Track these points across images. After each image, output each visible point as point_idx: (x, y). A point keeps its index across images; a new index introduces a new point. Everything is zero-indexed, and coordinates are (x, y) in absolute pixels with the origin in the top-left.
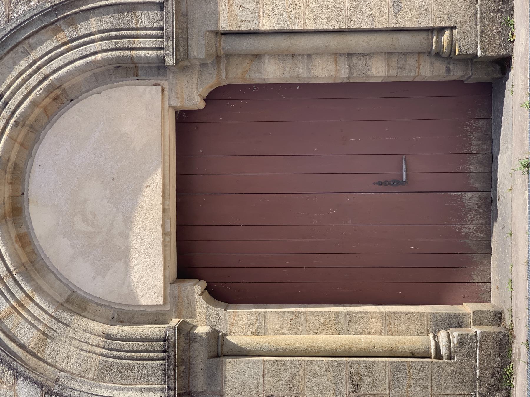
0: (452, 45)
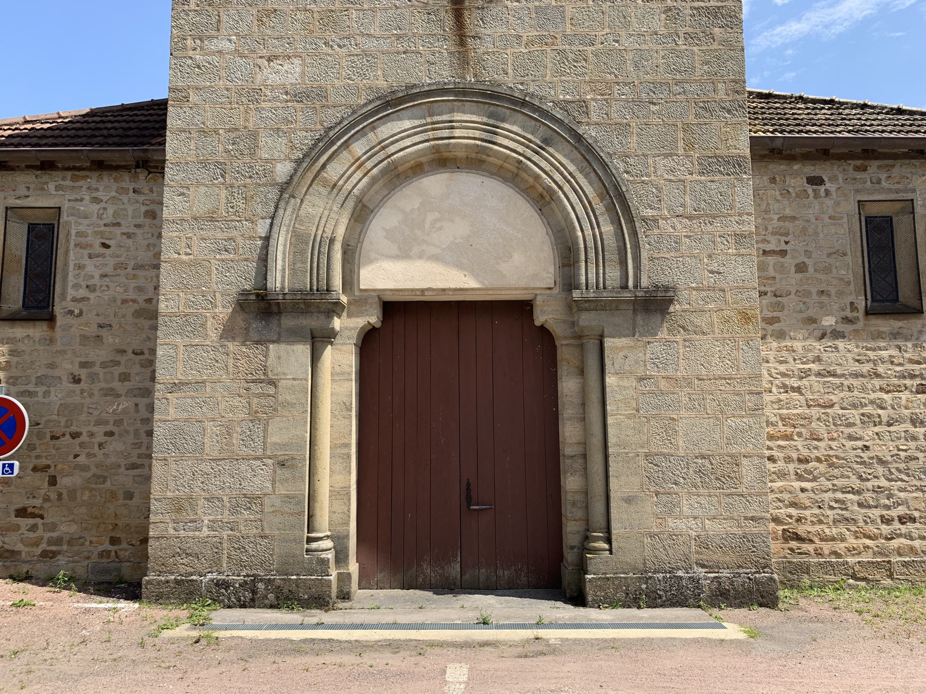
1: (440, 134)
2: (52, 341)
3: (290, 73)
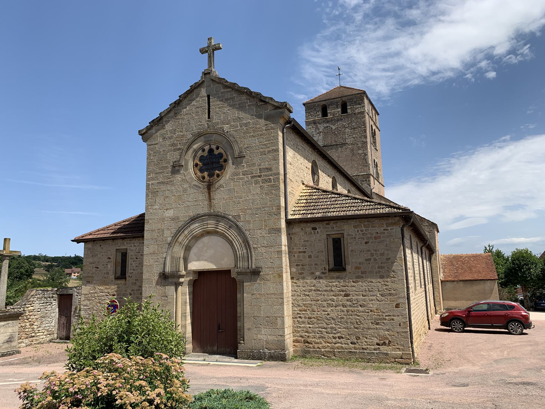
0: (240, 343)
1: (205, 227)
2: (126, 284)
3: (170, 213)
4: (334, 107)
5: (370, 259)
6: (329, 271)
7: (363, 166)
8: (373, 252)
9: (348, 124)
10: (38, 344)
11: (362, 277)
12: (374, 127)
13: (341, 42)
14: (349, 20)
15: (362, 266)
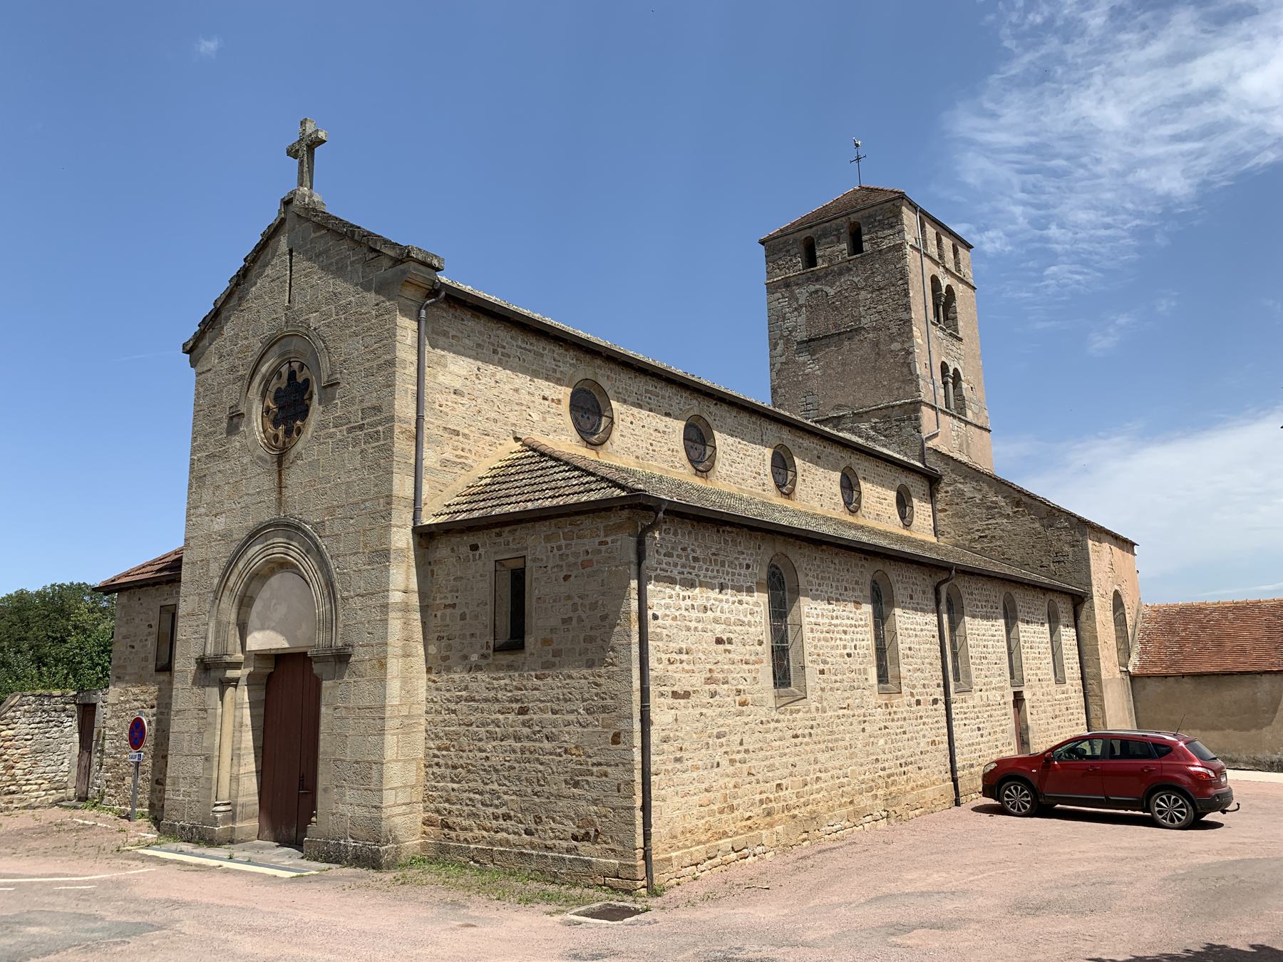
4: (832, 242)
5: (571, 618)
6: (495, 650)
7: (903, 381)
8: (576, 600)
9: (866, 280)
10: (25, 808)
11: (553, 665)
12: (945, 281)
13: (1054, 85)
14: (1071, 30)
15: (555, 636)
